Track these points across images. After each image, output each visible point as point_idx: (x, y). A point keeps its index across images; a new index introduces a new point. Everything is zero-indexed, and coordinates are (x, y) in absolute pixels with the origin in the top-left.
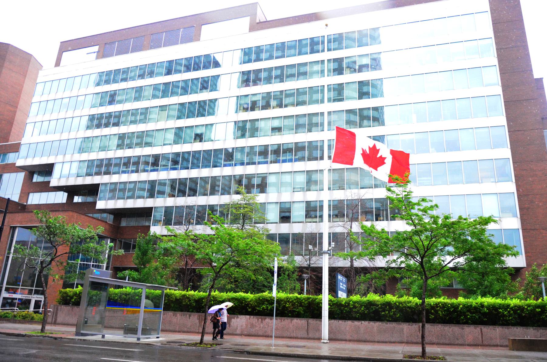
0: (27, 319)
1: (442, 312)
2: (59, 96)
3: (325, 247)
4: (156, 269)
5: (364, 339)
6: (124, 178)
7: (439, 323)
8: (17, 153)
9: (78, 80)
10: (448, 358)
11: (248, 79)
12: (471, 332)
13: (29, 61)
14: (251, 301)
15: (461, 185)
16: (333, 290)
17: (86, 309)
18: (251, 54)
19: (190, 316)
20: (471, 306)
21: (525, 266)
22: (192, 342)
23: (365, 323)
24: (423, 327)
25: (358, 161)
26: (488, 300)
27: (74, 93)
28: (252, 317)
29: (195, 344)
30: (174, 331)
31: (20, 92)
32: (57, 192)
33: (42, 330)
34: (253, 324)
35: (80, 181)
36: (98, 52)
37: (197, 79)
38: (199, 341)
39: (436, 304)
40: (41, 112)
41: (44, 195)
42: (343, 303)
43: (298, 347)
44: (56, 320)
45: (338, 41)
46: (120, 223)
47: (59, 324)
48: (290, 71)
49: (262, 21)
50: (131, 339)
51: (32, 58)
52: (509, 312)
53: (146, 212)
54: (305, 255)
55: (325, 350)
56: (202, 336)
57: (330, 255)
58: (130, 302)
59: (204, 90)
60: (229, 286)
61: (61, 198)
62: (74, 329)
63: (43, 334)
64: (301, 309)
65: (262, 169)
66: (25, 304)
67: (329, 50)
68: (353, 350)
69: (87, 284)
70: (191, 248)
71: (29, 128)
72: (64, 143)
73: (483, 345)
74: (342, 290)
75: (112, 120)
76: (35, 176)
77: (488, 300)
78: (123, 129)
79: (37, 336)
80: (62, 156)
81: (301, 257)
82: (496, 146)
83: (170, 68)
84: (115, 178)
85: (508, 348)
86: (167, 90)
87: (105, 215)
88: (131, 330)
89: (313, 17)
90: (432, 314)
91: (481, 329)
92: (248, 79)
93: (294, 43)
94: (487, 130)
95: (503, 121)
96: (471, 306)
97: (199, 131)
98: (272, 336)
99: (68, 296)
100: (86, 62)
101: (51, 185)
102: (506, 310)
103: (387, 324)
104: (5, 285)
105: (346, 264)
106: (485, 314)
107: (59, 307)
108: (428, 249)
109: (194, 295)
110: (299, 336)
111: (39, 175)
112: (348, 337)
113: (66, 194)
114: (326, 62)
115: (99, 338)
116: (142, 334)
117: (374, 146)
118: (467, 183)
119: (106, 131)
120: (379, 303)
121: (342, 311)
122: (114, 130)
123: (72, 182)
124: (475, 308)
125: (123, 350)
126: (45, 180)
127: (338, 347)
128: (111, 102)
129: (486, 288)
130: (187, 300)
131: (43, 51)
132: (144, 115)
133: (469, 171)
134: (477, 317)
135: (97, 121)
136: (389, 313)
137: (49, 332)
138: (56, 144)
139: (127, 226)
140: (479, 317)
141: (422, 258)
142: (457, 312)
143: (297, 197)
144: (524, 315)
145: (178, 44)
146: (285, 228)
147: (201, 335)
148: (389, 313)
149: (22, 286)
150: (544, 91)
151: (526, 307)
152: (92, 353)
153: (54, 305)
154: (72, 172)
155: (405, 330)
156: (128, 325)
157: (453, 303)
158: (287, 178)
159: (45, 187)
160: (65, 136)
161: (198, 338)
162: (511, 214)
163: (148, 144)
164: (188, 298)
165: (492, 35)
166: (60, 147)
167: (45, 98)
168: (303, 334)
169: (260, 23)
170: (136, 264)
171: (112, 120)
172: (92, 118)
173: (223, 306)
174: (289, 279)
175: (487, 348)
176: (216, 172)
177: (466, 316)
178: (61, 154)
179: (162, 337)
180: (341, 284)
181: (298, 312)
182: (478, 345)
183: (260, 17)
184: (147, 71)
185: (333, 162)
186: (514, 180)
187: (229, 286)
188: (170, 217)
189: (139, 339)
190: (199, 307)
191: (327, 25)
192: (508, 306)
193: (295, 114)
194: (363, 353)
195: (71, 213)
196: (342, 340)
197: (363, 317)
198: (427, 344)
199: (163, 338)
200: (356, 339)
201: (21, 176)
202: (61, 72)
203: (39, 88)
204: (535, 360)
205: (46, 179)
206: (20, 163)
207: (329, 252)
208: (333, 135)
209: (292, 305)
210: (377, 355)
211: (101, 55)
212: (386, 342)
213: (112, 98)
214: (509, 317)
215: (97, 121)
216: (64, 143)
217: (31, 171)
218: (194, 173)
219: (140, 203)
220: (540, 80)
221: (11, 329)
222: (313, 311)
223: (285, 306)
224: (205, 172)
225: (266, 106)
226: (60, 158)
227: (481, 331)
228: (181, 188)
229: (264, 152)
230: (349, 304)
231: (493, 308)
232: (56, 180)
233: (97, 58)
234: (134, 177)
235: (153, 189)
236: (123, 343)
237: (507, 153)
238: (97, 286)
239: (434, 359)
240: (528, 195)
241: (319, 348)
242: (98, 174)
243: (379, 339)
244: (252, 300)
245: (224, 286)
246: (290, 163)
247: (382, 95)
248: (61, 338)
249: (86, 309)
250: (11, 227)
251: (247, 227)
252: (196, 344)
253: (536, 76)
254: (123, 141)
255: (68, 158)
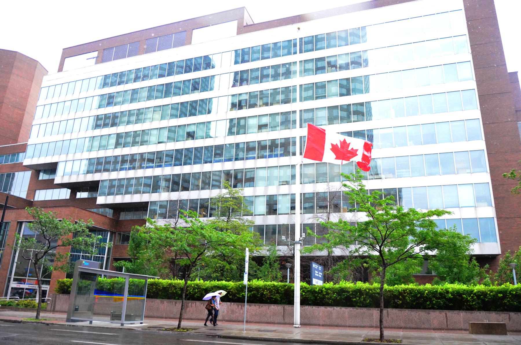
0: (29, 307)
1: (409, 298)
2: (62, 99)
3: (297, 237)
4: (149, 260)
5: (336, 324)
6: (122, 174)
7: (407, 308)
8: (25, 153)
9: (79, 84)
10: (404, 342)
11: (240, 79)
12: (436, 316)
13: (36, 67)
14: (231, 289)
15: (437, 177)
16: (306, 276)
17: (76, 297)
18: (242, 56)
19: (176, 303)
20: (437, 291)
21: (500, 253)
22: (171, 327)
23: (337, 309)
24: (381, 312)
25: (329, 156)
26: (457, 286)
27: (76, 96)
28: (233, 303)
29: (172, 330)
30: (162, 318)
31: (28, 96)
32: (62, 189)
33: (37, 317)
34: (233, 310)
35: (81, 179)
36: (97, 57)
37: (189, 81)
38: (177, 327)
39: (404, 290)
40: (66, 112)
41: (50, 191)
42: (317, 290)
43: (268, 331)
44: (54, 309)
45: (313, 42)
46: (119, 217)
47: (57, 312)
48: (255, 74)
49: (249, 24)
50: (116, 325)
51: (38, 64)
52: (472, 297)
53: (142, 207)
54: (291, 245)
55: (297, 333)
56: (180, 322)
57: (301, 245)
58: (112, 291)
59: (196, 91)
60: (214, 275)
61: (65, 194)
62: (65, 316)
63: (38, 321)
64: (278, 296)
65: (249, 164)
66: (31, 293)
67: (301, 52)
68: (320, 334)
69: (76, 274)
70: (168, 240)
71: (34, 130)
72: (66, 143)
73: (448, 329)
74: (318, 278)
75: (112, 120)
76: (41, 174)
77: (457, 286)
78: (121, 129)
79: (33, 322)
80: (65, 156)
81: (286, 247)
82: (471, 138)
83: (170, 69)
84: (114, 175)
85: (468, 332)
86: (167, 90)
87: (107, 210)
88: (116, 317)
89: (299, 19)
90: (400, 299)
91: (446, 314)
92: (240, 79)
93: (311, 38)
94: (462, 123)
95: (477, 113)
96: (437, 291)
97: (191, 129)
98: (245, 321)
99: (65, 285)
100: (85, 66)
101: (56, 182)
102: (469, 295)
103: (357, 309)
104: (13, 276)
105: (324, 253)
106: (450, 300)
107: (58, 296)
108: (385, 239)
109: (180, 284)
110: (276, 321)
111: (44, 173)
112: (321, 323)
113: (69, 191)
114: (298, 63)
115: (87, 323)
116: (126, 320)
117: (345, 140)
118: (444, 174)
119: (106, 131)
120: (351, 290)
121: (316, 297)
122: (113, 130)
123: (74, 179)
124: (441, 294)
125: (100, 334)
126: (50, 178)
127: (307, 331)
128: (109, 104)
129: (455, 274)
130: (173, 288)
131: (47, 56)
132: (139, 115)
133: (443, 163)
134: (442, 303)
135: (101, 122)
136: (360, 299)
137: (44, 318)
138: (60, 144)
139: (124, 219)
140: (445, 303)
141: (380, 247)
142: (423, 298)
143: (281, 191)
144: (486, 300)
145: (155, 51)
146: (271, 220)
147: (178, 320)
148: (360, 299)
149: (29, 277)
150: (519, 84)
151: (489, 293)
152: (64, 336)
153: (53, 294)
154: (74, 170)
155: (374, 315)
156: (115, 312)
157: (420, 289)
158: (276, 172)
159: (50, 185)
160: (67, 137)
161: (176, 323)
162: (486, 204)
163: (143, 143)
164: (174, 286)
165: (466, 32)
166: (64, 147)
167: (49, 101)
168: (280, 319)
169: (247, 26)
170: (130, 255)
171: (112, 120)
172: (98, 118)
173: (216, 294)
174: (271, 268)
175: (452, 331)
176: (207, 168)
177: (431, 302)
178: (64, 154)
179: (145, 323)
180: (317, 272)
181: (275, 299)
182: (443, 329)
183: (247, 21)
184: (140, 75)
185: (304, 157)
186: (489, 171)
187: (214, 275)
188: (173, 210)
189: (122, 325)
190: (197, 295)
191: (299, 29)
192: (472, 291)
193: (280, 112)
194: (327, 337)
195: (72, 208)
196: (315, 325)
197: (336, 303)
198: (386, 327)
199: (146, 323)
200: (328, 323)
201: (28, 174)
202: (64, 77)
203: (44, 92)
204: (487, 343)
205: (51, 177)
206: (27, 162)
207: (300, 242)
208: (304, 132)
209: (270, 292)
210: (339, 339)
211: (100, 60)
212: (357, 327)
213: (110, 100)
214: (472, 302)
215: (101, 122)
216: (66, 143)
217: (37, 169)
218: (186, 169)
219: (137, 198)
220: (514, 74)
221: (10, 316)
222: (287, 298)
223: (262, 294)
224: (197, 168)
225: (252, 106)
226: (63, 157)
227: (446, 316)
228: (179, 183)
229: (250, 148)
230: (322, 291)
231: (458, 294)
232: (60, 178)
233: (97, 63)
234: (131, 174)
235: (154, 184)
236: (107, 328)
237: (481, 144)
238: (85, 276)
239: (391, 342)
240: (504, 185)
241: (291, 333)
242: (97, 171)
243: (351, 323)
244: (232, 287)
245: (210, 273)
246: (276, 158)
247: (367, 91)
248: (53, 324)
249: (76, 297)
250: (18, 222)
251: (232, 219)
252: (175, 328)
253: (509, 71)
254: (120, 140)
255: (70, 157)
